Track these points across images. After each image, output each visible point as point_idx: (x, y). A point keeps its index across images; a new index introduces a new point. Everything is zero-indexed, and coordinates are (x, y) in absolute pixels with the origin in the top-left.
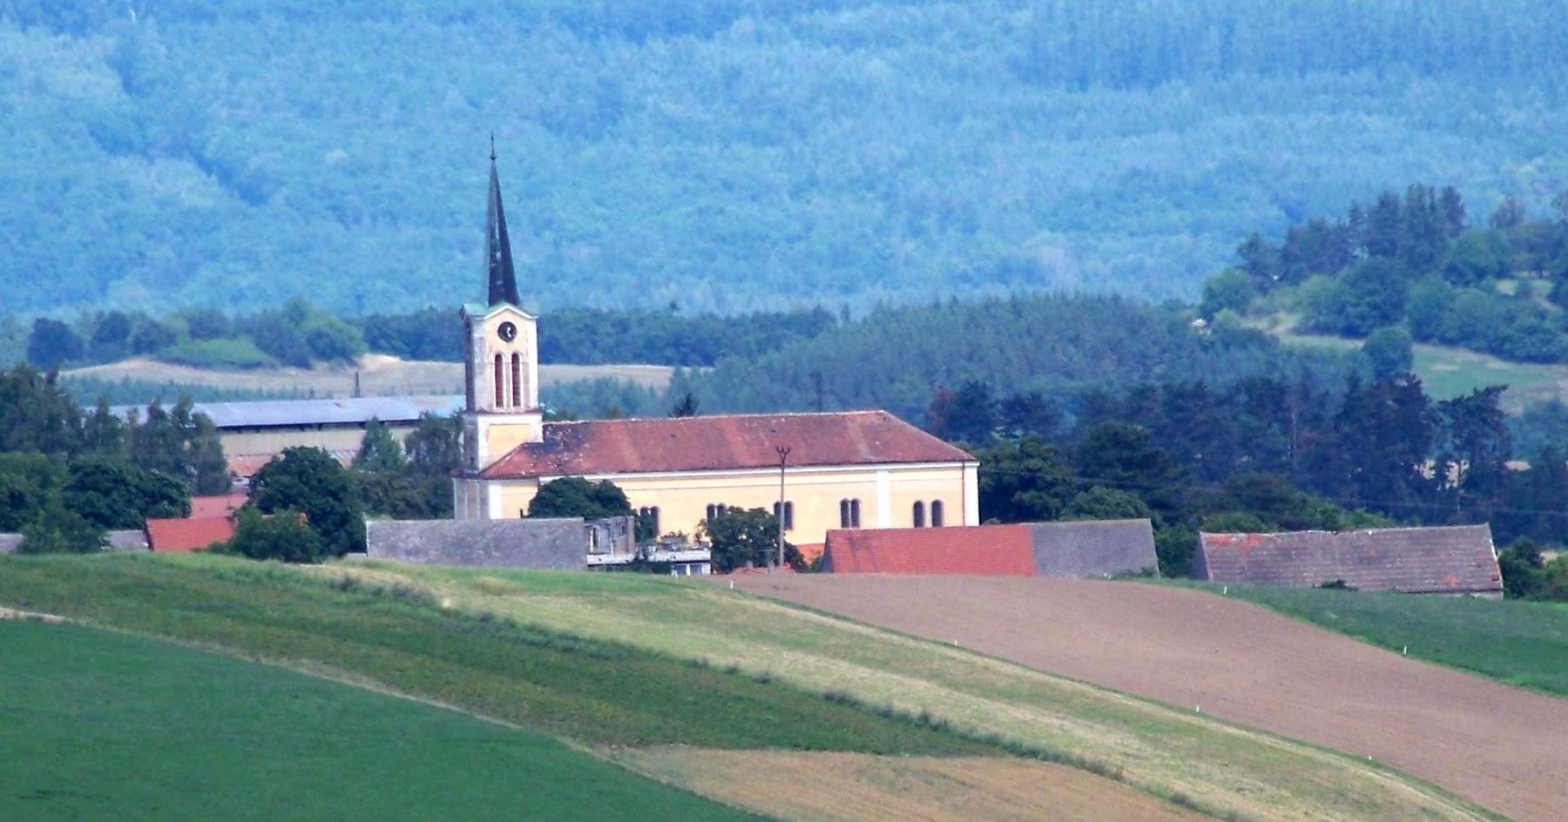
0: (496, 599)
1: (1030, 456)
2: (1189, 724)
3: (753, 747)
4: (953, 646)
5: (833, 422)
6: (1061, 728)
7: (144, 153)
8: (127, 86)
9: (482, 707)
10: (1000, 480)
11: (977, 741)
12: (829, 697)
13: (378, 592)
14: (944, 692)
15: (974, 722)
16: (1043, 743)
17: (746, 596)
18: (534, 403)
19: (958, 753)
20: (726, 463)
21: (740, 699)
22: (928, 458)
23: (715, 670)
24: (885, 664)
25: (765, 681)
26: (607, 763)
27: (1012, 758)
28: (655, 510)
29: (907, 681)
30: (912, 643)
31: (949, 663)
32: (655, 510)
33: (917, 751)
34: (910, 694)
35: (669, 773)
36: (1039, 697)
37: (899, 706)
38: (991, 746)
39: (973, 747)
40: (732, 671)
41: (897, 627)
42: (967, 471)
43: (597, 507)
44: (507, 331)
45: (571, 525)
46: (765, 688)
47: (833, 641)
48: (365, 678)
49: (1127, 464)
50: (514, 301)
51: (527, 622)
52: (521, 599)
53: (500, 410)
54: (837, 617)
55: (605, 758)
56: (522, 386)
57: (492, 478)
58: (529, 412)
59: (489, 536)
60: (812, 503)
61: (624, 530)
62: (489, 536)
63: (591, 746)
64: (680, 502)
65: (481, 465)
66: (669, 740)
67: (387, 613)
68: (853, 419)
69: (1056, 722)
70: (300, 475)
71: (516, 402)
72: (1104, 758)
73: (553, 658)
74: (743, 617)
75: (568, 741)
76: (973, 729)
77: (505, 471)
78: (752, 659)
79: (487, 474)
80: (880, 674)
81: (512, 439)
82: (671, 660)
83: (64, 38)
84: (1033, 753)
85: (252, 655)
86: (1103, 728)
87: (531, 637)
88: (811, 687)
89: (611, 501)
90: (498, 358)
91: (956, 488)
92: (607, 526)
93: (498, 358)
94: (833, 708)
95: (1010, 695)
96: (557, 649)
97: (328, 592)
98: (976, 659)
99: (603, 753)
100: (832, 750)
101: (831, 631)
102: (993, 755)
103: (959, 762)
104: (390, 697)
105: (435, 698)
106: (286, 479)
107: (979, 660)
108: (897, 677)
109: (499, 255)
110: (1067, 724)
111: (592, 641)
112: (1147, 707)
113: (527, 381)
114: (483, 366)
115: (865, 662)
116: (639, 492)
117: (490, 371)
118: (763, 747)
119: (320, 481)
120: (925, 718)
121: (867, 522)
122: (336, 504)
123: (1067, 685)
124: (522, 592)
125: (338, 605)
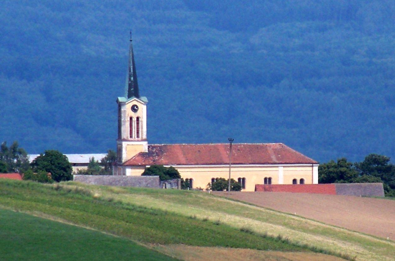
0: (116, 195)
1: (341, 166)
2: (384, 244)
3: (210, 246)
4: (294, 215)
5: (262, 147)
6: (333, 243)
7: (53, 126)
8: (49, 100)
9: (104, 229)
10: (329, 176)
11: (299, 246)
12: (242, 230)
13: (70, 191)
14: (288, 230)
15: (299, 240)
16: (325, 248)
17: (215, 197)
18: (145, 137)
19: (291, 250)
20: (219, 163)
21: (207, 230)
22: (298, 162)
23: (198, 220)
24: (267, 220)
25: (218, 224)
26: (152, 250)
27: (313, 253)
28: (191, 180)
29: (274, 226)
30: (279, 214)
31: (292, 221)
32: (191, 180)
33: (275, 249)
34: (274, 230)
35: (176, 254)
36: (325, 233)
37: (269, 234)
38: (305, 248)
39: (298, 248)
40: (205, 220)
41: (273, 208)
42: (314, 167)
43: (167, 176)
44: (134, 109)
45: (154, 179)
46: (218, 226)
47: (247, 212)
48: (59, 219)
49: (379, 170)
50: (137, 96)
51: (127, 202)
52: (126, 195)
53: (131, 139)
54: (250, 204)
55: (150, 248)
56: (140, 130)
57: (127, 166)
58: (143, 140)
59: (122, 182)
60: (253, 176)
61: (177, 183)
62: (122, 182)
63: (145, 244)
64: (201, 177)
65: (123, 161)
66: (177, 242)
67: (72, 198)
68: (270, 147)
69: (331, 241)
70: (51, 161)
71: (138, 137)
72: (349, 254)
73: (135, 214)
74: (213, 203)
75: (136, 242)
76: (297, 243)
77: (131, 163)
78: (213, 217)
79: (126, 164)
80: (264, 223)
81: (136, 151)
82: (181, 216)
83: (24, 81)
84: (321, 251)
85: (16, 209)
86: (350, 244)
87: (127, 207)
88: (236, 227)
89: (173, 174)
90: (131, 118)
91: (310, 174)
92: (170, 183)
93: (131, 118)
94: (243, 233)
95: (314, 232)
96: (137, 211)
97: (50, 190)
98: (302, 219)
99: (151, 246)
100: (241, 248)
101: (247, 209)
102: (305, 251)
103: (291, 253)
104: (69, 225)
105: (86, 226)
106: (46, 163)
107: (304, 220)
108: (271, 225)
109: (132, 78)
110: (335, 242)
111: (151, 209)
112: (368, 237)
113: (142, 128)
114: (125, 122)
115: (258, 219)
116: (185, 173)
117: (128, 124)
118: (213, 246)
119: (59, 164)
120: (279, 238)
121: (274, 182)
122: (65, 173)
123: (337, 229)
124: (127, 193)
125: (53, 195)
